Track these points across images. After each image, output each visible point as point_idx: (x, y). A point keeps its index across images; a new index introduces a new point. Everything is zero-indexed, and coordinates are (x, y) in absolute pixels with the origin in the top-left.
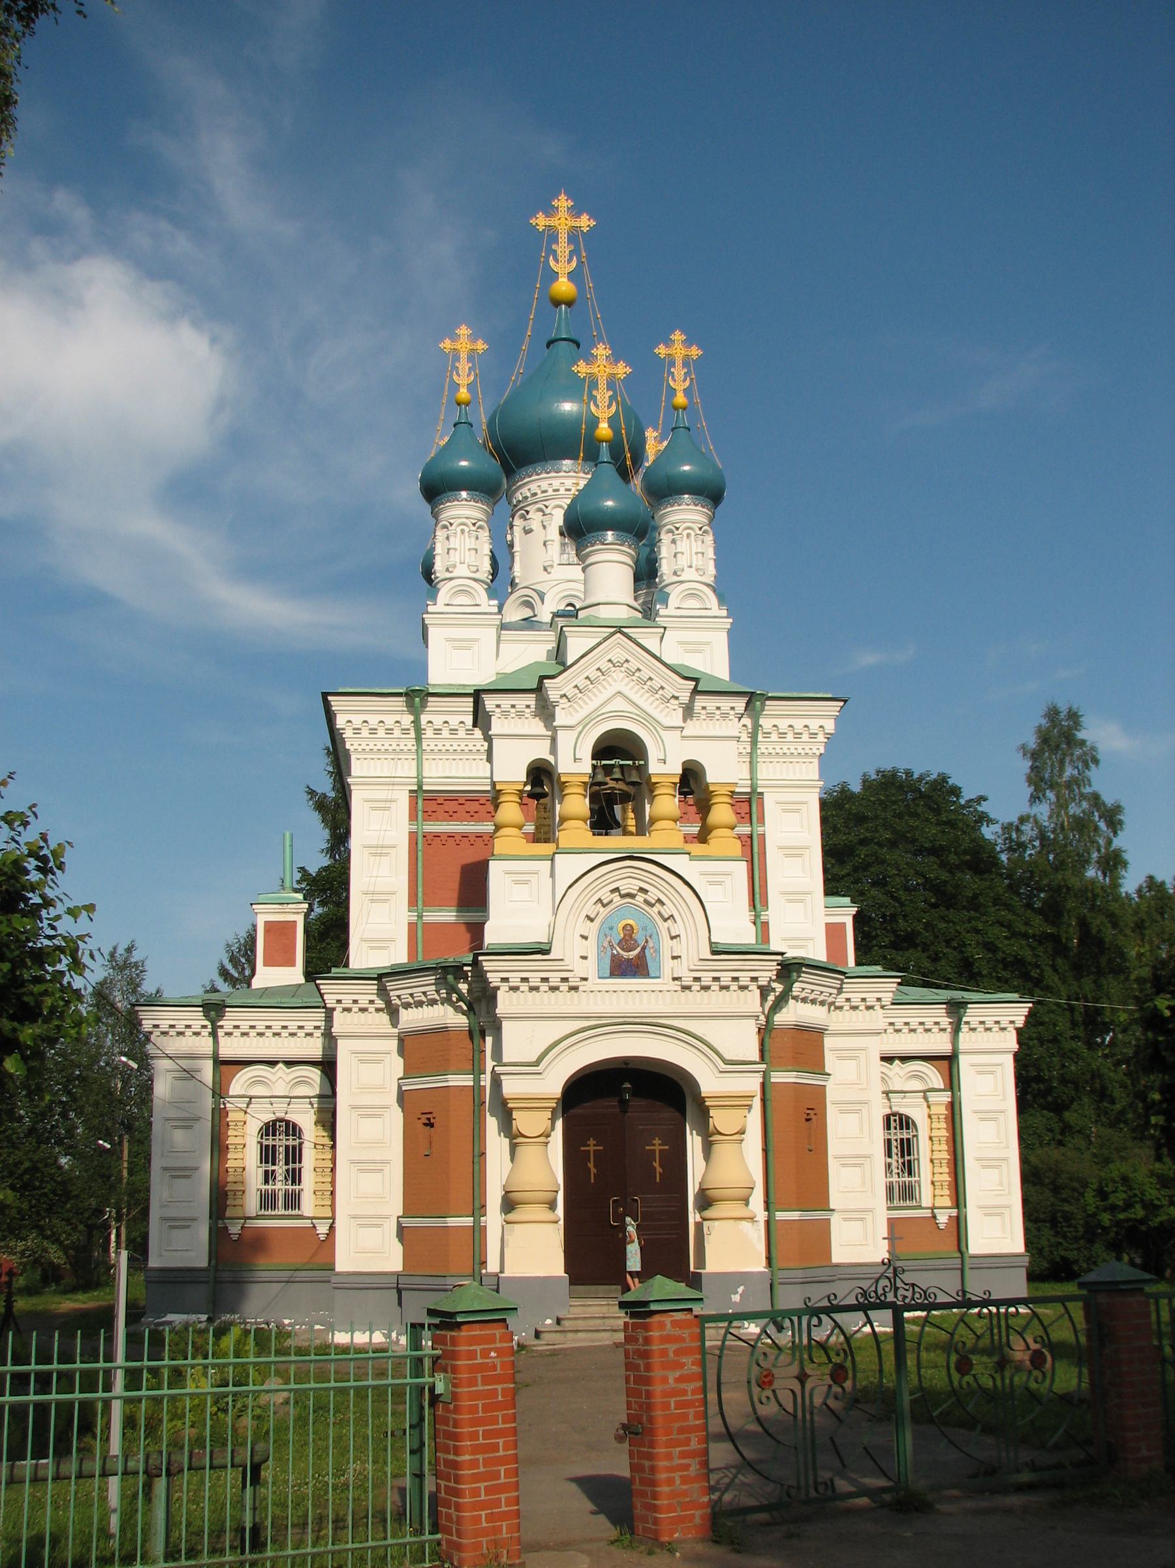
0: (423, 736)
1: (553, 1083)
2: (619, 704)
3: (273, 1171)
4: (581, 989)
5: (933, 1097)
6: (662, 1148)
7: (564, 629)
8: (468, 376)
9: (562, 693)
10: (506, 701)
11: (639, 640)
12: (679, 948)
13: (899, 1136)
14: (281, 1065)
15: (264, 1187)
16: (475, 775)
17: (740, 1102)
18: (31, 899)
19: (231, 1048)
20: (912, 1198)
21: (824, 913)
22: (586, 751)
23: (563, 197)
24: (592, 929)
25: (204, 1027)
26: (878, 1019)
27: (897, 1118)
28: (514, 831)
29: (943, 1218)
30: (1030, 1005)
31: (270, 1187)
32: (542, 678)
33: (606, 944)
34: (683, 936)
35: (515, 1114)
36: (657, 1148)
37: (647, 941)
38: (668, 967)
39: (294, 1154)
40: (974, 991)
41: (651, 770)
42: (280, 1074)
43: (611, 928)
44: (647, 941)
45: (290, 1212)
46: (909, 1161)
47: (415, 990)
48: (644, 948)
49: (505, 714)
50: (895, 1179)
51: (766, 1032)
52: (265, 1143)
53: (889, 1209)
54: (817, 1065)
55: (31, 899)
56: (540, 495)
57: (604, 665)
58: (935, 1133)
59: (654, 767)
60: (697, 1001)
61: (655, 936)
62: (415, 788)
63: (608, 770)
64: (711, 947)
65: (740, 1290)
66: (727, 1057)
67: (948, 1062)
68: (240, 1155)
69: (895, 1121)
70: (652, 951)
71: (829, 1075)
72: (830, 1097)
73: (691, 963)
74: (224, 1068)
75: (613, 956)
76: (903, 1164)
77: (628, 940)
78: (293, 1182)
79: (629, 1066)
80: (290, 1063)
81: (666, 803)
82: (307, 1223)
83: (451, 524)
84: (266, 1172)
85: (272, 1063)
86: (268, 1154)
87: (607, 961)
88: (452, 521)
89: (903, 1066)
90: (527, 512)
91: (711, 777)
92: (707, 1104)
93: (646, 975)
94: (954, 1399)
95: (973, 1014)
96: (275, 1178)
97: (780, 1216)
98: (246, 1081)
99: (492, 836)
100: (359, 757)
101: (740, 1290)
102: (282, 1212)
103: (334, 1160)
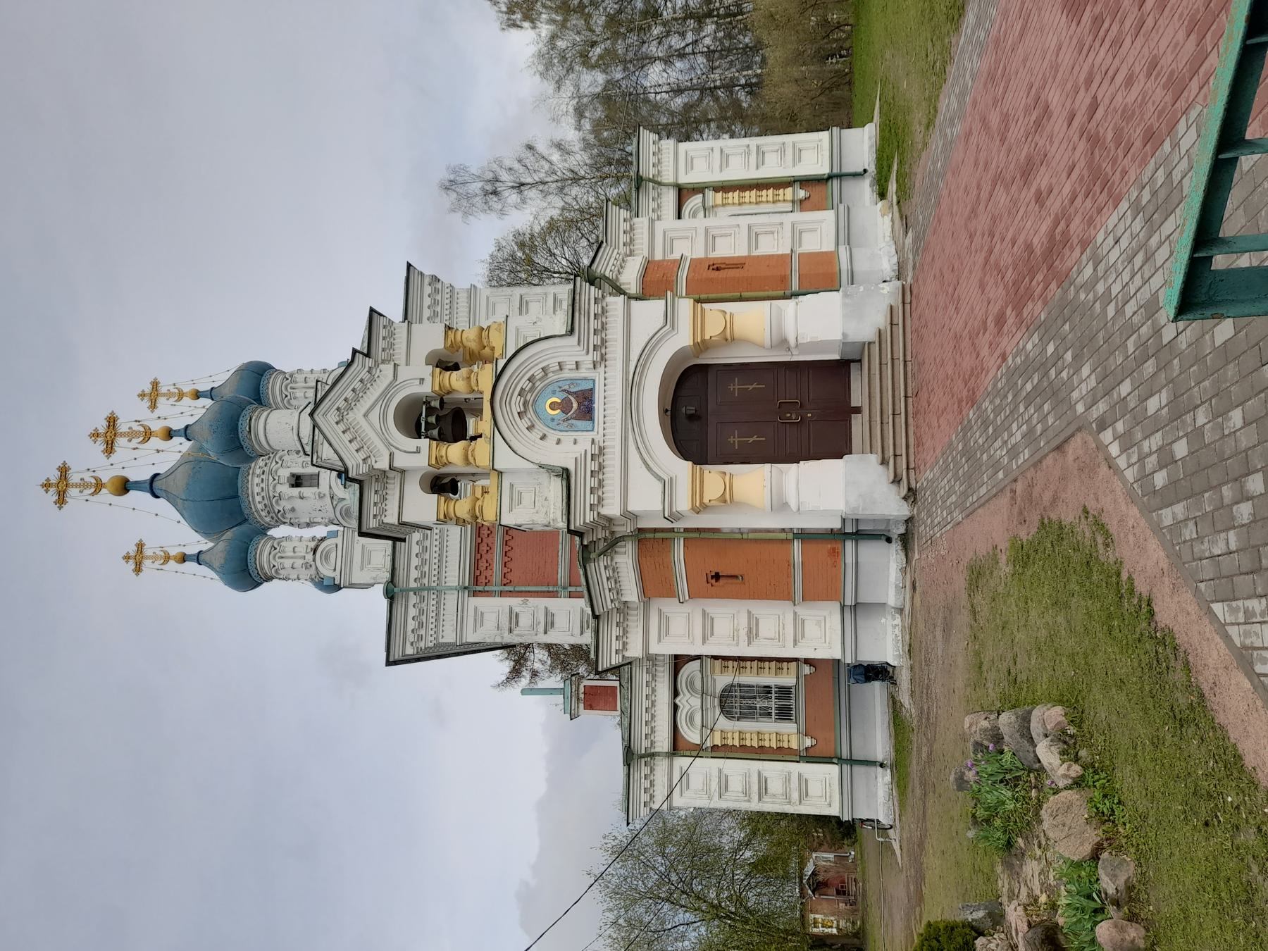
0: (427, 585)
1: (681, 469)
2: (374, 416)
5: (710, 202)
7: (314, 463)
9: (361, 462)
10: (371, 510)
14: (677, 701)
19: (663, 742)
22: (413, 443)
24: (553, 436)
28: (479, 503)
29: (802, 194)
30: (641, 128)
33: (566, 424)
36: (737, 387)
38: (584, 372)
43: (553, 420)
56: (266, 502)
57: (342, 427)
58: (736, 201)
59: (426, 389)
60: (615, 351)
62: (466, 592)
63: (429, 426)
66: (661, 324)
67: (683, 193)
68: (730, 735)
74: (680, 744)
75: (575, 418)
77: (564, 406)
80: (676, 693)
81: (456, 381)
82: (802, 680)
83: (274, 566)
85: (675, 708)
86: (748, 713)
90: (279, 511)
93: (592, 391)
98: (689, 728)
103: (752, 659)
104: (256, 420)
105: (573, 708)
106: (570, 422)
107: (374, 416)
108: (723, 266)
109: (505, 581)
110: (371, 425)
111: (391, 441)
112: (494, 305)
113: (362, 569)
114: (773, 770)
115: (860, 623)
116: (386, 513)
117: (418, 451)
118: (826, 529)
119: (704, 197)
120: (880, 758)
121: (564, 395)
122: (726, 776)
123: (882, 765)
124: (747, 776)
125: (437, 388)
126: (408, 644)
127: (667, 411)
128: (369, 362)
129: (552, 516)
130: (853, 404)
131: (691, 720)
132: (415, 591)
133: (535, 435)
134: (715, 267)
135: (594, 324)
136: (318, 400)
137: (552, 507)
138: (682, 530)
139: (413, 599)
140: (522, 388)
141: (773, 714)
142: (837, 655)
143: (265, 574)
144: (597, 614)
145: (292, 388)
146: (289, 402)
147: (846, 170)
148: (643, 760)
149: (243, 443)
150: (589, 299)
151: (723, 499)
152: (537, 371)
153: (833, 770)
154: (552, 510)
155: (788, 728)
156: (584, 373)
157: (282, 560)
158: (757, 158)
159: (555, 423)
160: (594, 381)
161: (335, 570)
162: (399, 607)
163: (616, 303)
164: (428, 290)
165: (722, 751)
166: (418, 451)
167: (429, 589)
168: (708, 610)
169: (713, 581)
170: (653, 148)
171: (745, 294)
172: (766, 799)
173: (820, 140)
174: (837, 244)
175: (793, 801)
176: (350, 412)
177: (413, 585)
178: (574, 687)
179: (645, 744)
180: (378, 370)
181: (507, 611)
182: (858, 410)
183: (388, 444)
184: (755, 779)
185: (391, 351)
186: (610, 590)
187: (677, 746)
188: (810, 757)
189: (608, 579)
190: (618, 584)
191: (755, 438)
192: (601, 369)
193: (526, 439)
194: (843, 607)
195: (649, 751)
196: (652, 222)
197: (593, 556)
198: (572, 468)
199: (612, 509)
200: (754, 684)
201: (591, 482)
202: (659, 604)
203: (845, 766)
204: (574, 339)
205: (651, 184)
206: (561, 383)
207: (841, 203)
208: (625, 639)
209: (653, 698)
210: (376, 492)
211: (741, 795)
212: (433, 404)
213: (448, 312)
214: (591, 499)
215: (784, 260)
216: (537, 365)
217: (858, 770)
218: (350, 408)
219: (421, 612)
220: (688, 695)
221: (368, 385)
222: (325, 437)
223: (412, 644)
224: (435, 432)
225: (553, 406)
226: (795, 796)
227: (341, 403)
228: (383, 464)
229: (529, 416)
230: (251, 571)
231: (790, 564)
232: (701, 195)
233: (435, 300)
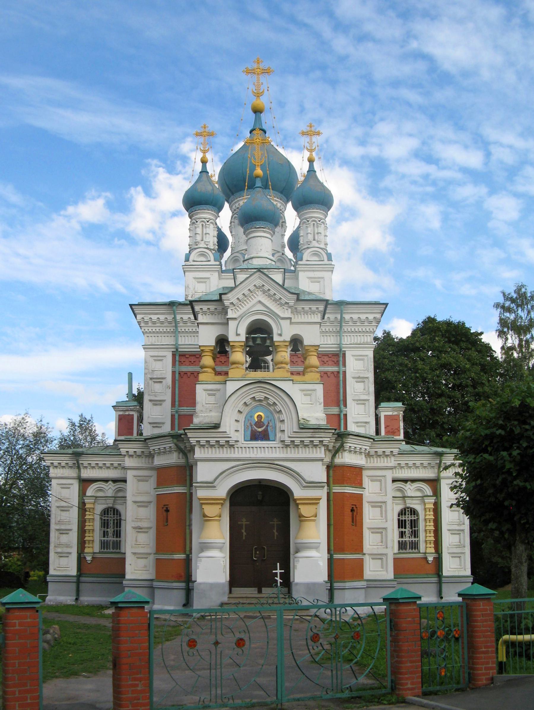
2: (260, 307)
3: (405, 532)
4: (236, 446)
5: (427, 500)
6: (278, 523)
11: (270, 276)
12: (284, 427)
13: (410, 519)
15: (401, 539)
16: (188, 343)
17: (315, 501)
19: (86, 474)
20: (415, 548)
24: (242, 418)
25: (74, 464)
26: (391, 462)
27: (409, 510)
29: (430, 559)
31: (404, 539)
32: (221, 295)
33: (249, 424)
34: (286, 421)
35: (300, 507)
36: (244, 523)
37: (269, 423)
39: (414, 524)
40: (423, 446)
41: (275, 339)
42: (110, 486)
43: (251, 417)
44: (269, 423)
45: (115, 550)
47: (161, 447)
48: (267, 426)
49: (205, 313)
51: (330, 467)
52: (103, 518)
54: (359, 484)
59: (276, 338)
60: (292, 453)
61: (273, 421)
62: (175, 350)
63: (254, 339)
64: (299, 426)
66: (308, 479)
69: (408, 511)
70: (271, 428)
71: (365, 488)
73: (289, 433)
75: (252, 430)
76: (412, 532)
77: (259, 423)
78: (117, 537)
79: (261, 484)
81: (285, 355)
84: (104, 532)
86: (105, 524)
87: (249, 433)
88: (197, 220)
89: (412, 484)
91: (306, 343)
94: (324, 651)
97: (336, 556)
98: (94, 489)
99: (198, 373)
100: (148, 335)
102: (112, 550)
104: (263, 231)
105: (120, 408)
106: (250, 427)
107: (260, 307)
108: (355, 513)
109: (182, 374)
110: (254, 306)
111: (244, 318)
112: (363, 360)
113: (195, 278)
114: (73, 538)
115: (147, 589)
116: (204, 315)
118: (192, 572)
120: (82, 598)
122: (68, 511)
123: (77, 599)
124: (69, 523)
125: (276, 344)
126: (142, 316)
128: (292, 303)
129: (200, 414)
130: (263, 589)
131: (100, 490)
132: (175, 318)
133: (240, 407)
134: (355, 509)
135: (307, 441)
137: (206, 415)
138: (191, 491)
139: (170, 318)
140: (269, 398)
141: (104, 539)
142: (127, 577)
143: (193, 216)
144: (147, 441)
145: (314, 224)
146: (304, 222)
147: (444, 586)
148: (76, 462)
149: (249, 224)
150: (321, 437)
151: (205, 516)
152: (279, 407)
153: (74, 572)
154: (203, 414)
155: (97, 548)
156: (279, 435)
157: (201, 226)
158: (456, 530)
159: (249, 418)
160: (274, 441)
161: (194, 261)
162: (163, 309)
163: (321, 452)
164: (371, 317)
165: (82, 508)
166: (238, 335)
167: (176, 326)
168: (152, 504)
169: (165, 509)
171: (332, 528)
172: (57, 533)
173: (465, 570)
174: (367, 581)
175: (56, 548)
176: (262, 292)
177: (178, 317)
178: (133, 408)
179: (86, 463)
180: (287, 308)
181: (163, 376)
182: (260, 591)
183: (242, 317)
184: (68, 527)
185: (302, 313)
186: (159, 449)
187: (85, 483)
188: (81, 559)
189: (165, 448)
190: (163, 453)
191: (245, 534)
192: (280, 445)
193: (239, 401)
194: (152, 580)
195: (81, 465)
197: (175, 441)
198: (220, 430)
199: (199, 453)
200: (121, 528)
201: (213, 441)
202: (154, 473)
203: (75, 578)
204: (296, 430)
205: (438, 462)
206: (273, 421)
207: (397, 583)
208: (135, 456)
209: (111, 468)
210: (216, 309)
211: (59, 519)
212: (268, 341)
213: (360, 330)
214: (203, 441)
215: (359, 548)
216: (283, 407)
217: (74, 586)
218: (264, 292)
219: (162, 323)
220: (114, 488)
221: (278, 303)
222: (251, 275)
223: (143, 318)
224: (251, 343)
225: (259, 417)
226: (59, 550)
227: (267, 287)
228: (230, 314)
229: (253, 403)
230: (194, 207)
231: (173, 552)
232: (432, 494)
233: (364, 321)
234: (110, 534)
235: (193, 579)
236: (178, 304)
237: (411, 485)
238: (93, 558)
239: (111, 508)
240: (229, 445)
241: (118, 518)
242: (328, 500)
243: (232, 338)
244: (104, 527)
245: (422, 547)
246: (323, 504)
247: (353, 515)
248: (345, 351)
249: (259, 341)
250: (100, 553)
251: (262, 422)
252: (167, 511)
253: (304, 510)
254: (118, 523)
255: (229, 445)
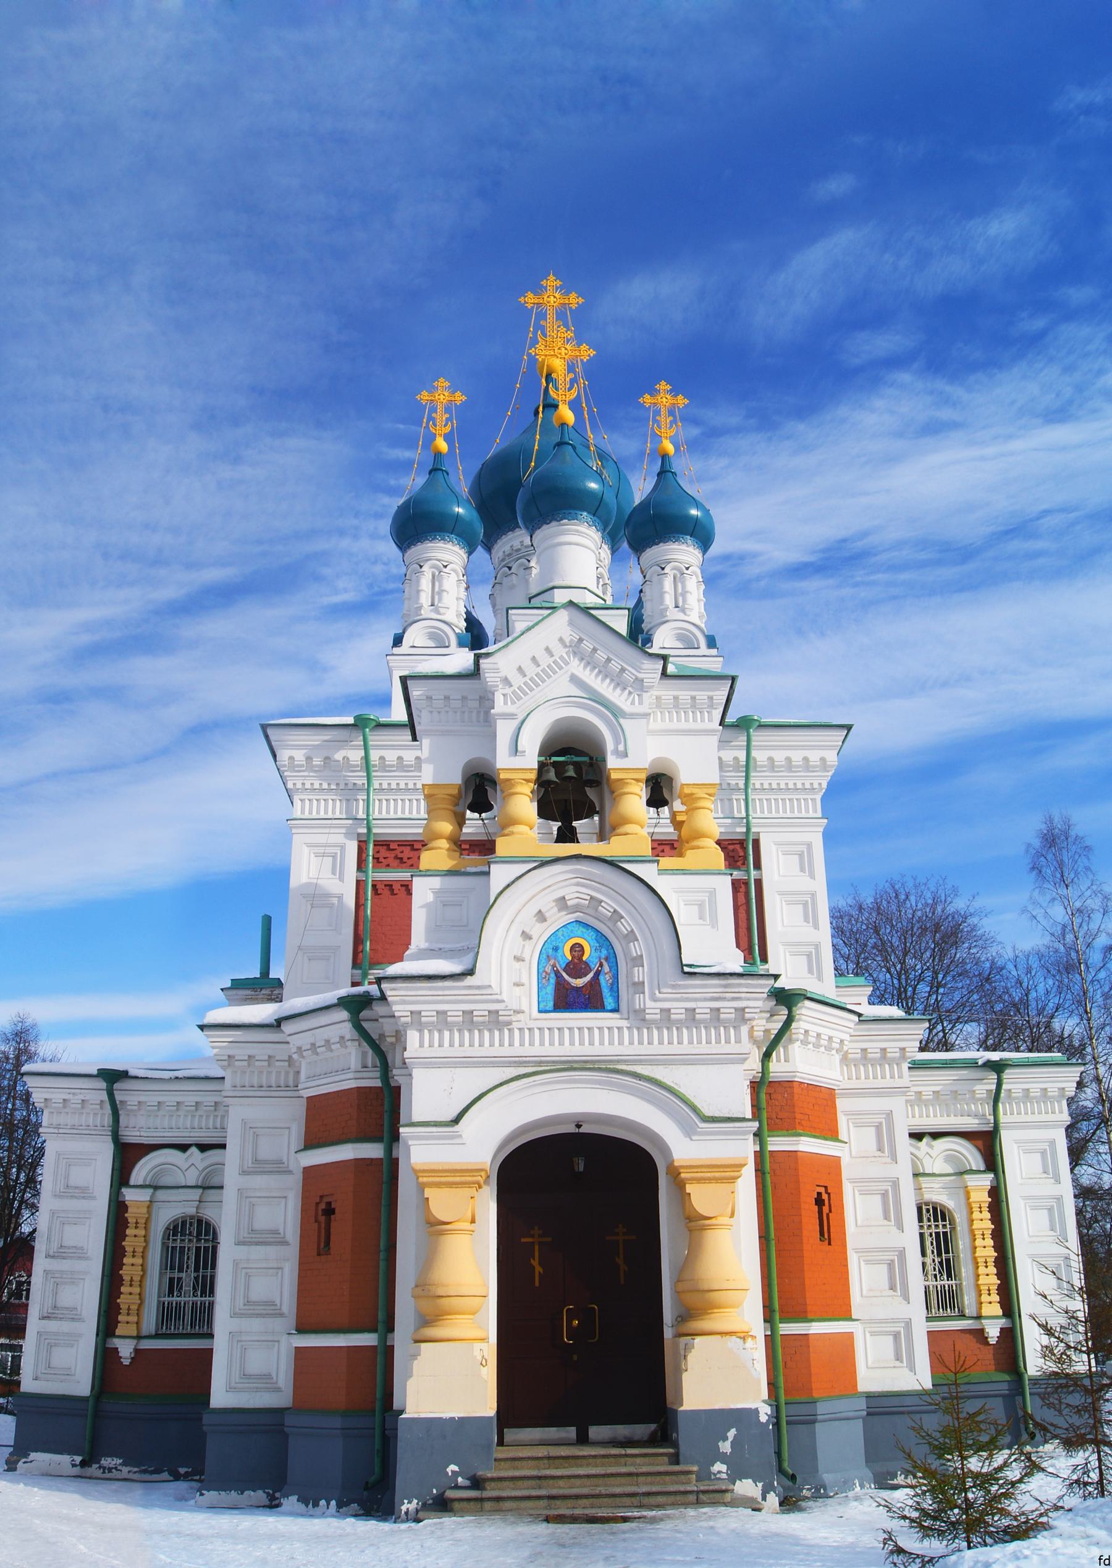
3: (180, 1279)
4: (515, 1025)
5: (972, 1181)
8: (445, 426)
13: (933, 1230)
14: (194, 1149)
17: (726, 1173)
18: (619, 1258)
21: (834, 985)
23: (552, 277)
29: (993, 1332)
33: (549, 969)
43: (556, 949)
44: (601, 965)
46: (948, 1261)
48: (598, 973)
50: (932, 1283)
53: (928, 1319)
55: (619, 1258)
65: (732, 1433)
66: (708, 1112)
69: (928, 1211)
72: (846, 1174)
76: (941, 1263)
77: (577, 966)
78: (203, 1293)
79: (582, 1130)
81: (635, 801)
84: (171, 1280)
86: (172, 1259)
87: (550, 989)
92: (683, 1175)
95: (1013, 1081)
96: (181, 1288)
101: (732, 1433)
106: (553, 975)
108: (825, 1209)
117: (515, 750)
119: (979, 1172)
121: (595, 967)
127: (579, 1126)
134: (825, 1197)
136: (592, 612)
138: (394, 1156)
159: (550, 951)
170: (1053, 1091)
177: (374, 756)
188: (105, 1358)
191: (538, 1270)
196: (902, 1090)
201: (455, 1010)
214: (429, 1011)
224: (552, 775)
234: (188, 1286)
235: (396, 1406)
236: (374, 724)
237: (931, 1147)
238: (136, 1351)
239: (192, 1217)
240: (496, 1021)
241: (210, 1244)
242: (760, 1171)
243: (503, 761)
244: (172, 1268)
245: (968, 1301)
246: (746, 1185)
247: (820, 1213)
248: (759, 833)
249: (571, 773)
250: (157, 1336)
251: (586, 963)
252: (329, 1211)
253: (701, 1198)
254: (207, 1259)
255: (496, 1021)
